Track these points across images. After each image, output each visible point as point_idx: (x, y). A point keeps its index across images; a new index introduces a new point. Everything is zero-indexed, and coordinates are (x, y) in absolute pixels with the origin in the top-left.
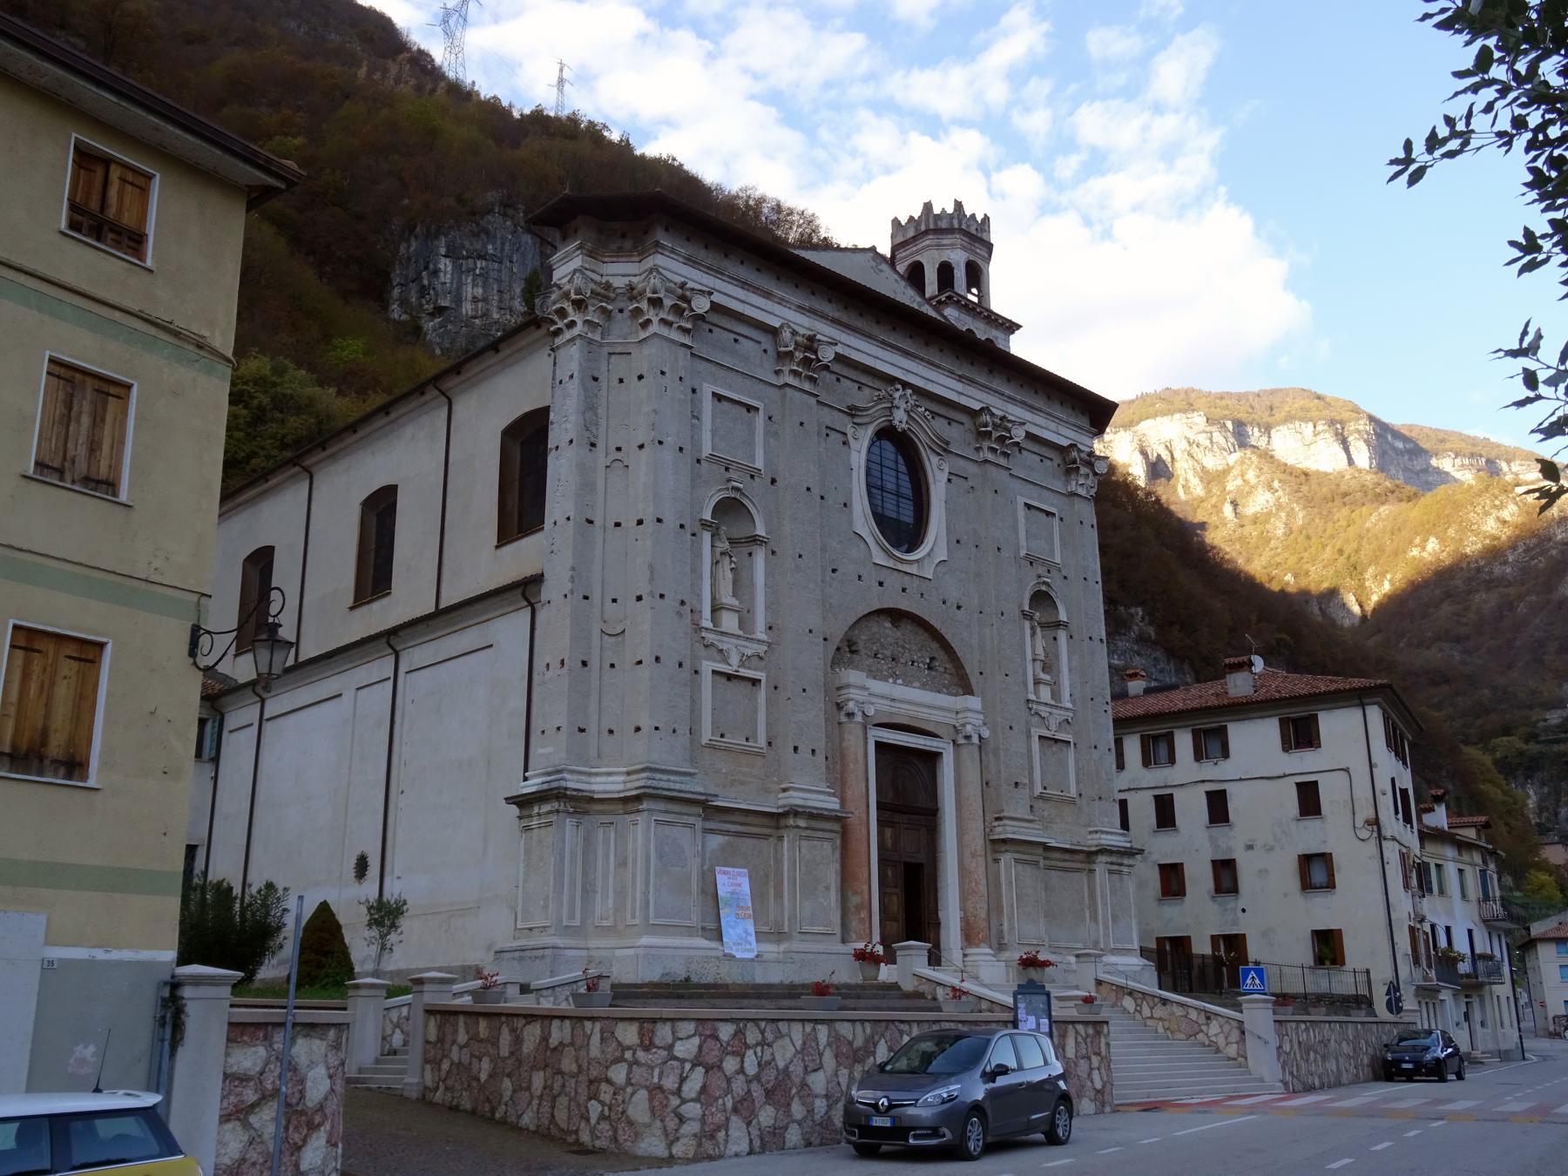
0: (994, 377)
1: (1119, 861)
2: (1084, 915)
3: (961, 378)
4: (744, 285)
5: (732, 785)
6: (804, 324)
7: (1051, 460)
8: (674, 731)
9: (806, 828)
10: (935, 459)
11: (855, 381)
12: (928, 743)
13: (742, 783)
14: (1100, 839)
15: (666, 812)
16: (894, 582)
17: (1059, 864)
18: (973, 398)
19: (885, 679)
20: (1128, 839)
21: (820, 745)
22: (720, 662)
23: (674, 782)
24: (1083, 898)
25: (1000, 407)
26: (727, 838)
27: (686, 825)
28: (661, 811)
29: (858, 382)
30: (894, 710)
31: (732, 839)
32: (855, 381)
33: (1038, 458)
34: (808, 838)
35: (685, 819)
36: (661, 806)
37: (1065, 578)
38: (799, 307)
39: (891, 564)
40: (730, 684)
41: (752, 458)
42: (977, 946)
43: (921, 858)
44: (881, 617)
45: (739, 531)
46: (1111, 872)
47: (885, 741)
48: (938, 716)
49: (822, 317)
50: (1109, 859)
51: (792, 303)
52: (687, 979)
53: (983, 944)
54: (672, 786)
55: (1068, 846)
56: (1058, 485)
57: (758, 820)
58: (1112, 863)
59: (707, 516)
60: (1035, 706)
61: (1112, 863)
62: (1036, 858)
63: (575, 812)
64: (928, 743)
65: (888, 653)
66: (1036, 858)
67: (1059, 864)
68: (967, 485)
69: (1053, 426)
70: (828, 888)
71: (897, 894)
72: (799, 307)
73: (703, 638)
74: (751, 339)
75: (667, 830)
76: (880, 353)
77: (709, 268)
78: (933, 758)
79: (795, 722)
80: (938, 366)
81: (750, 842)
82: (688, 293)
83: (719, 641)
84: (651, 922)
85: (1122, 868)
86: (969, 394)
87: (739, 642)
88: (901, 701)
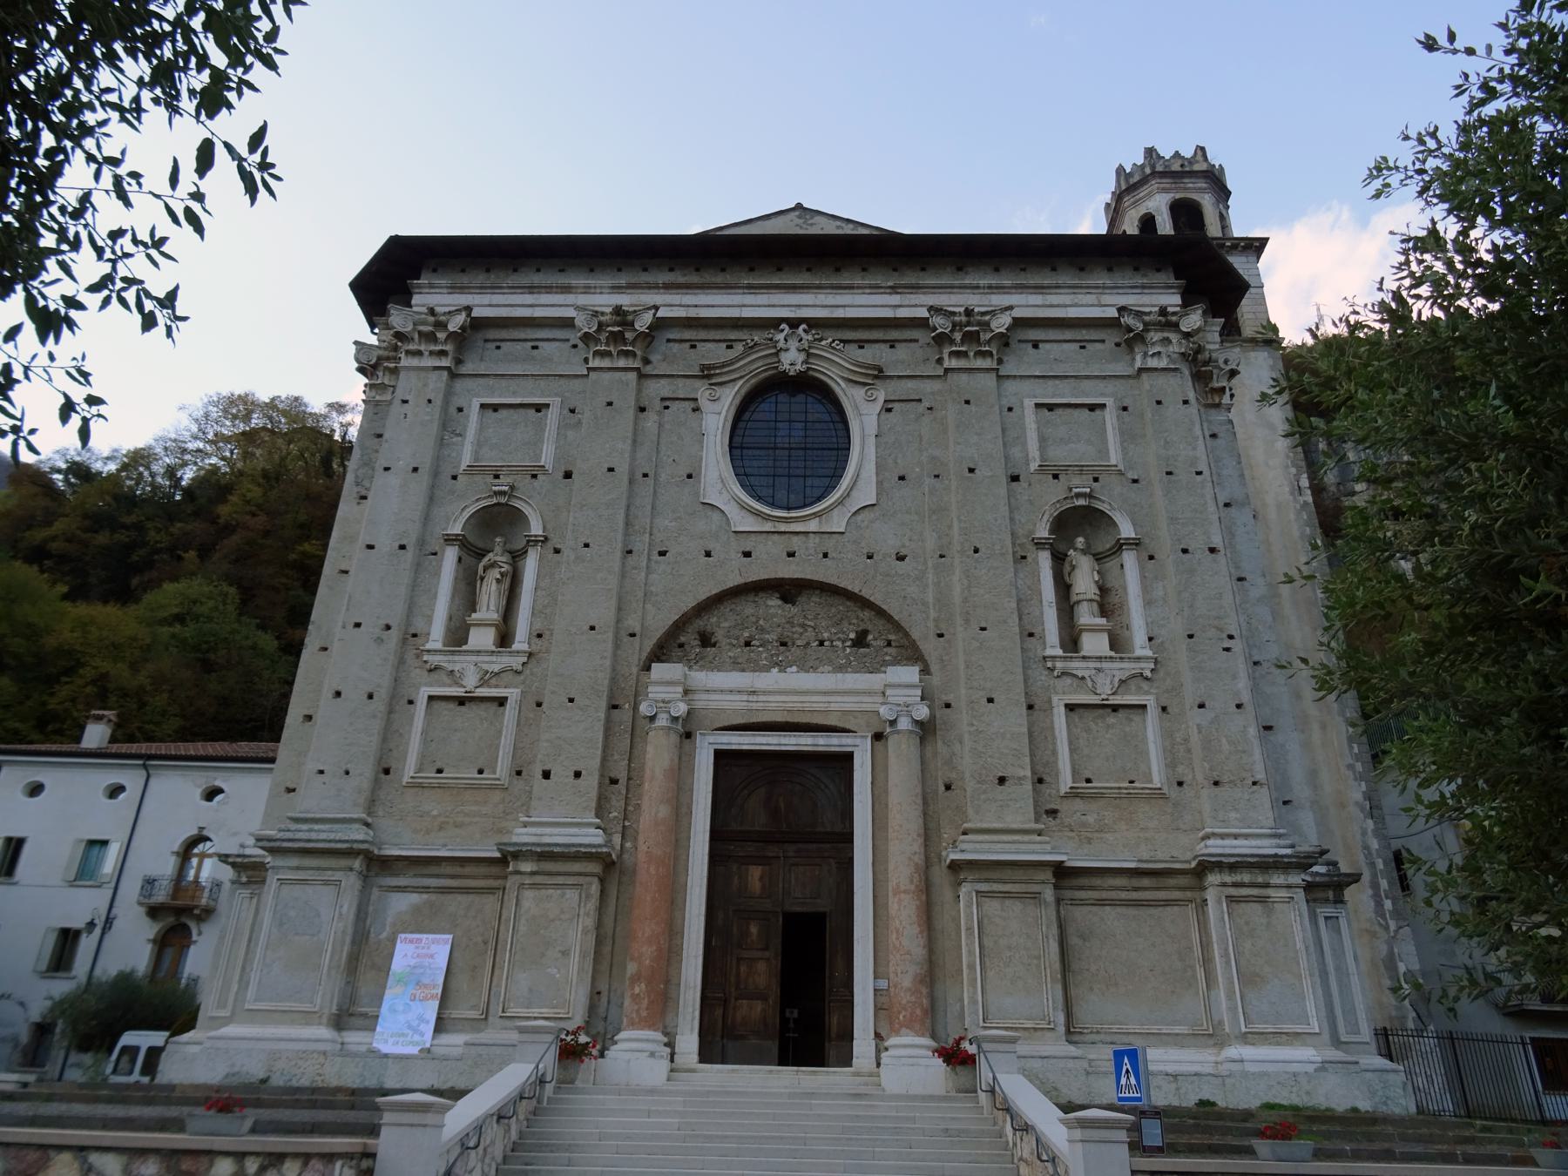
0: (966, 273)
1: (1260, 880)
2: (1194, 976)
3: (894, 290)
4: (532, 289)
5: (441, 828)
6: (605, 301)
7: (1103, 341)
8: (347, 773)
9: (533, 873)
10: (859, 393)
11: (720, 341)
12: (821, 741)
13: (457, 825)
14: (1206, 846)
15: (298, 868)
16: (777, 547)
17: (1123, 895)
18: (913, 306)
19: (767, 669)
20: (1288, 842)
21: (592, 765)
22: (450, 686)
23: (319, 831)
24: (1190, 948)
25: (956, 301)
26: (425, 896)
27: (326, 883)
28: (290, 868)
29: (725, 341)
30: (755, 706)
31: (433, 897)
32: (720, 341)
33: (1076, 346)
34: (534, 886)
35: (328, 875)
36: (294, 861)
37: (1135, 481)
38: (613, 288)
39: (768, 527)
40: (463, 708)
41: (1104, 452)
42: (897, 1033)
43: (823, 905)
44: (761, 594)
45: (1104, 544)
46: (1231, 899)
47: (734, 747)
48: (849, 704)
49: (650, 288)
50: (1228, 879)
51: (601, 287)
52: (264, 1081)
53: (904, 1030)
54: (314, 836)
55: (1132, 865)
56: (1120, 368)
57: (483, 870)
58: (1235, 885)
59: (1043, 532)
60: (1059, 665)
61: (1235, 885)
62: (1036, 888)
63: (249, 882)
64: (821, 741)
65: (772, 637)
66: (1036, 888)
67: (1123, 895)
68: (921, 407)
69: (1091, 299)
70: (566, 953)
71: (768, 960)
72: (613, 288)
73: (426, 662)
74: (554, 340)
75: (297, 891)
76: (749, 299)
77: (481, 288)
78: (844, 761)
79: (547, 741)
80: (851, 287)
81: (463, 899)
82: (442, 318)
83: (449, 662)
84: (246, 1007)
85: (1270, 892)
86: (913, 303)
87: (480, 658)
88: (765, 693)
